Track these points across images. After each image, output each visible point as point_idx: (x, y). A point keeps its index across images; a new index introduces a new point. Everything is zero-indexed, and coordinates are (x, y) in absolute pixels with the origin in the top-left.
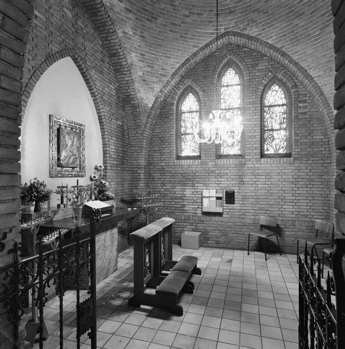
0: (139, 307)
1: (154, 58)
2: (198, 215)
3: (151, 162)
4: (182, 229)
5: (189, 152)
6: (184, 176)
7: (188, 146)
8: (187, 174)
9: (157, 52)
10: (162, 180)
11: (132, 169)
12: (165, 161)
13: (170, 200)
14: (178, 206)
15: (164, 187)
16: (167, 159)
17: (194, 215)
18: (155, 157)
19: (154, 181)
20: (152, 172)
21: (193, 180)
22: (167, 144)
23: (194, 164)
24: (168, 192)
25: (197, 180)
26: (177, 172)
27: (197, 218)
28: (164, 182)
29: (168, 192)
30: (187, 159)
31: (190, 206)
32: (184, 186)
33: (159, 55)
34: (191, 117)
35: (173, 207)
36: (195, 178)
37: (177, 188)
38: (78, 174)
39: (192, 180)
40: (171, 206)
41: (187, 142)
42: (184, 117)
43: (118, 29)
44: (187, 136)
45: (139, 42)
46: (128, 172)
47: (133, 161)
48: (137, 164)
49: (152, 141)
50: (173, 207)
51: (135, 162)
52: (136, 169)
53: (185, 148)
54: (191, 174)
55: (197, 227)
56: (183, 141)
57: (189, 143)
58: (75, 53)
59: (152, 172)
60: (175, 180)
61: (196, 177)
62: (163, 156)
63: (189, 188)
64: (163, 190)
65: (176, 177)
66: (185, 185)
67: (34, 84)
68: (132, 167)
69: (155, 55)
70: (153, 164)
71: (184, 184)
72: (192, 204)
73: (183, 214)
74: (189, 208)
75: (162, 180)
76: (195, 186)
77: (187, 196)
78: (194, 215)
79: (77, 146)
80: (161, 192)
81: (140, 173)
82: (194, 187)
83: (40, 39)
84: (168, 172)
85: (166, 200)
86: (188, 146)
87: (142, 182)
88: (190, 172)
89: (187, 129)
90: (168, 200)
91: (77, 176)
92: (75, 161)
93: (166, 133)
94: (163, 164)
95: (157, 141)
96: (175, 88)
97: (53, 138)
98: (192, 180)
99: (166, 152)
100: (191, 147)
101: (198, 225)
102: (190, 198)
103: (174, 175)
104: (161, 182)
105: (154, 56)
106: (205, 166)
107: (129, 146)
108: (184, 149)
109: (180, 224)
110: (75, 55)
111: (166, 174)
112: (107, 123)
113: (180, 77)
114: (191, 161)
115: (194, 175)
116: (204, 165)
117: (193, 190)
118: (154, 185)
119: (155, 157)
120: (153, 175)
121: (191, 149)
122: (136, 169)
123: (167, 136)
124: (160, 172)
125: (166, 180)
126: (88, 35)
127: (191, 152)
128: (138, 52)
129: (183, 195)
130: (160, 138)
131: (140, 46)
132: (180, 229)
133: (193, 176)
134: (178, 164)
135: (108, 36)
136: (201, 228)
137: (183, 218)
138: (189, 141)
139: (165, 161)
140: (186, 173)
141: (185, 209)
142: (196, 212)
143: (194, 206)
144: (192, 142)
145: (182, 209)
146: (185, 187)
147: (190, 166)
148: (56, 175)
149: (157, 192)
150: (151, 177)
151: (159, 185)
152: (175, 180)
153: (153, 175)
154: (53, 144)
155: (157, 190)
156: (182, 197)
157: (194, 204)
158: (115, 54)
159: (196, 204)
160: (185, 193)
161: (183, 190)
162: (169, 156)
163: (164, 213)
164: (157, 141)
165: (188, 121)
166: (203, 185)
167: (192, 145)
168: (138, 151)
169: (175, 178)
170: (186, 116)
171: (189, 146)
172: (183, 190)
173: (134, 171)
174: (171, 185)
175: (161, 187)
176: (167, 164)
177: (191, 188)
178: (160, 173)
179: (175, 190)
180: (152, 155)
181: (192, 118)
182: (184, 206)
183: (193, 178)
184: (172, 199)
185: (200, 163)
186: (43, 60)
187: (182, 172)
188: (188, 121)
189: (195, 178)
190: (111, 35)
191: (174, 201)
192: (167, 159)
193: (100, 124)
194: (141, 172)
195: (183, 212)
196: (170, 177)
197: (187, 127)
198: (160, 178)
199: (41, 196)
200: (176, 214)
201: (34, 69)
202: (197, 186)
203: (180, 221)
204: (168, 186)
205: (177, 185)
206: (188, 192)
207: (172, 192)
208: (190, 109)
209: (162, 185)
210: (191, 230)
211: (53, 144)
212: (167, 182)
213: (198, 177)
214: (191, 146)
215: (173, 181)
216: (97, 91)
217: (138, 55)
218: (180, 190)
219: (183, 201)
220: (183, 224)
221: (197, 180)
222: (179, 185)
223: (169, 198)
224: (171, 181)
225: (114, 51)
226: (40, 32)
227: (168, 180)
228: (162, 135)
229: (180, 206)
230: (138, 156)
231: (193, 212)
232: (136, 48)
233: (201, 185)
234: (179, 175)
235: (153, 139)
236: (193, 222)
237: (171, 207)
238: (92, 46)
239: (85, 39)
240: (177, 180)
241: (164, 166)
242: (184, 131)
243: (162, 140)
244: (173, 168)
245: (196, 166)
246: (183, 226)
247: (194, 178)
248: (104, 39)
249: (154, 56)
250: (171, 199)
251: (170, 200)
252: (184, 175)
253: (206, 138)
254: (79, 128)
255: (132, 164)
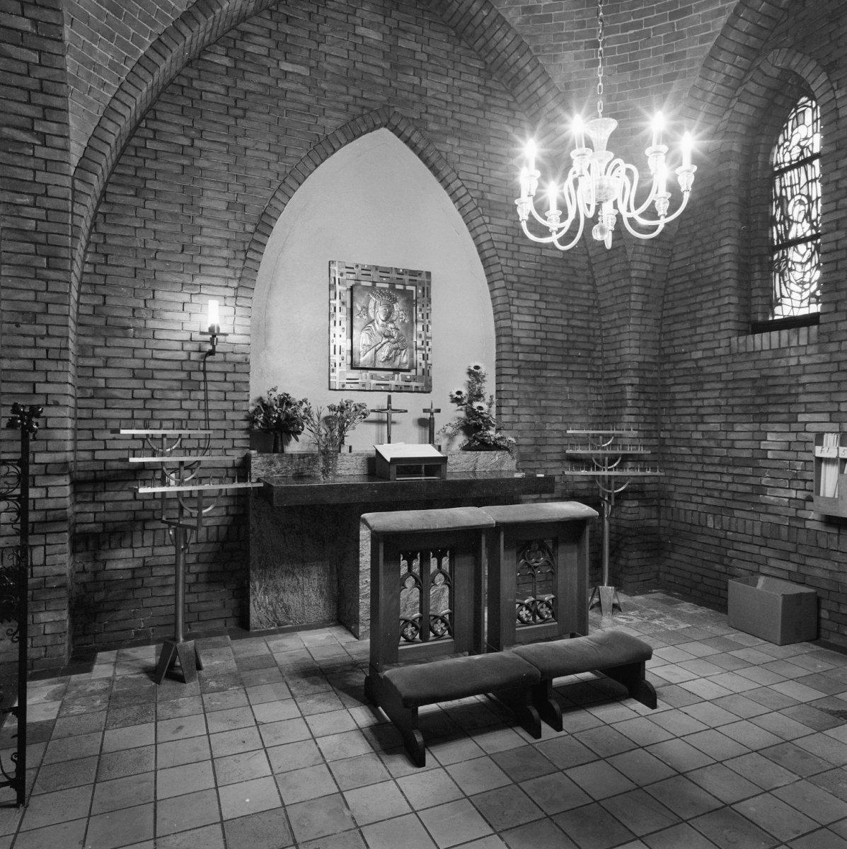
0: (376, 706)
1: (633, 37)
2: (809, 525)
3: (667, 351)
4: (755, 567)
5: (797, 304)
6: (761, 388)
7: (793, 287)
8: (770, 382)
9: (642, 13)
10: (696, 403)
11: (606, 377)
12: (704, 345)
13: (719, 469)
14: (742, 488)
15: (701, 427)
16: (710, 337)
17: (794, 523)
18: (677, 334)
19: (675, 408)
20: (670, 381)
21: (791, 399)
22: (711, 289)
23: (794, 343)
24: (712, 444)
25: (803, 398)
26: (739, 376)
27: (803, 537)
28: (703, 411)
29: (712, 444)
30: (788, 328)
31: (781, 492)
32: (760, 423)
33: (648, 23)
34: (803, 180)
35: (727, 491)
36: (797, 394)
37: (738, 428)
38: (407, 384)
39: (789, 399)
40: (719, 485)
41: (790, 270)
42: (781, 188)
43: (507, 10)
44: (791, 250)
45: (578, 13)
46: (593, 383)
47: (608, 353)
48: (618, 359)
49: (670, 290)
50: (727, 491)
51: (612, 354)
52: (614, 375)
53: (785, 293)
54: (784, 381)
55: (803, 570)
56: (777, 271)
57: (797, 275)
58: (391, 114)
59: (670, 381)
60: (732, 401)
61: (801, 390)
62: (699, 330)
63: (777, 427)
64: (698, 436)
65: (737, 392)
66: (764, 419)
67: (280, 207)
68: (607, 368)
69: (639, 25)
70: (673, 358)
71: (761, 416)
72: (785, 483)
73: (755, 517)
74: (780, 496)
75: (696, 403)
76: (796, 422)
77: (770, 455)
78: (794, 523)
79: (403, 322)
80: (693, 443)
81: (625, 385)
82: (794, 427)
83: (294, 116)
84: (712, 378)
85: (706, 469)
86: (793, 287)
87: (628, 411)
88: (779, 372)
89: (790, 226)
90: (711, 469)
91: (403, 389)
92: (396, 356)
93: (706, 256)
94: (699, 354)
95: (682, 287)
96: (734, 101)
97: (335, 308)
98: (789, 399)
99: (708, 316)
100: (807, 286)
101: (809, 562)
102: (779, 464)
103: (731, 386)
104: (693, 410)
105: (632, 32)
106: (833, 347)
107: (596, 312)
108: (782, 296)
109: (747, 548)
110: (389, 119)
111: (707, 386)
112: (499, 257)
113: (738, 58)
114: (784, 333)
115: (793, 382)
116: (830, 342)
117: (792, 437)
118: (674, 419)
119: (677, 334)
120: (674, 389)
121: (806, 294)
122: (614, 375)
123: (710, 263)
124: (691, 379)
125: (706, 403)
126: (432, 61)
127: (805, 303)
128: (581, 43)
129: (757, 454)
130: (689, 274)
131: (582, 24)
132: (749, 566)
133: (791, 385)
134: (742, 349)
135: (488, 41)
136: (818, 573)
137: (757, 531)
138: (799, 267)
139: (704, 345)
140: (767, 377)
141: (762, 498)
142: (801, 513)
143: (793, 494)
144: (808, 266)
145: (754, 499)
146: (763, 427)
147: (779, 352)
148: (343, 386)
149: (682, 442)
150: (668, 397)
151: (688, 419)
152: (732, 401)
153: (674, 389)
154: (335, 322)
155: (683, 435)
156: (754, 459)
157: (795, 484)
158: (516, 76)
159: (801, 485)
160: (763, 445)
161: (758, 436)
162: (715, 328)
163: (701, 508)
164: (682, 287)
165: (793, 196)
166: (825, 417)
167: (806, 279)
168: (619, 322)
169: (733, 397)
170: (788, 183)
171: (798, 284)
172: (758, 436)
173: (611, 379)
174: (722, 418)
175: (692, 427)
176: (709, 354)
177: (784, 427)
178: (691, 384)
179: (732, 436)
180: (670, 332)
181: (808, 182)
182: (761, 490)
183: (790, 394)
184: (723, 465)
185: (814, 339)
186: (304, 155)
187: (755, 375)
188: (793, 196)
189: (797, 394)
190: (492, 33)
191: (731, 471)
192: (710, 337)
193: (483, 264)
194: (626, 382)
195: (758, 509)
196: (716, 394)
197: (789, 220)
198: (690, 400)
199: (275, 421)
200: (737, 513)
201: (281, 178)
202: (806, 423)
203: (747, 539)
204: (714, 424)
205: (738, 418)
206: (774, 441)
207: (725, 444)
208: (802, 153)
209: (695, 419)
210: (785, 575)
211: (335, 322)
212: (710, 410)
213: (810, 388)
214: (804, 283)
215: (727, 405)
216: (463, 185)
217: (582, 50)
218: (748, 436)
219: (758, 472)
220: (756, 550)
221: (803, 398)
222: (744, 418)
223: (716, 460)
224: (720, 406)
225: (514, 71)
226: (294, 101)
227: (713, 402)
228: (696, 264)
229: (748, 489)
230: (619, 338)
231: (792, 512)
232: (570, 36)
233: (817, 417)
234: (744, 384)
235: (671, 282)
236: (790, 547)
237: (722, 491)
238: (448, 81)
239: (423, 73)
240: (739, 401)
241: (700, 359)
242: (779, 236)
243: (694, 281)
244: (727, 364)
245: (802, 351)
246: (756, 558)
247: (793, 391)
248: (483, 53)
249: (632, 32)
250: (719, 465)
251: (719, 469)
252: (759, 383)
253: (554, 233)
254: (410, 280)
255: (606, 360)
